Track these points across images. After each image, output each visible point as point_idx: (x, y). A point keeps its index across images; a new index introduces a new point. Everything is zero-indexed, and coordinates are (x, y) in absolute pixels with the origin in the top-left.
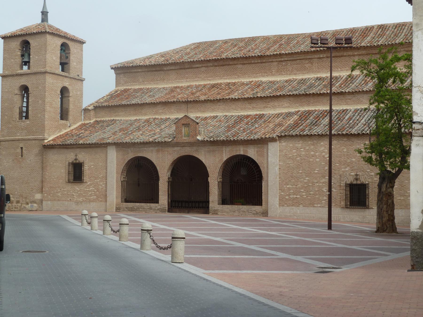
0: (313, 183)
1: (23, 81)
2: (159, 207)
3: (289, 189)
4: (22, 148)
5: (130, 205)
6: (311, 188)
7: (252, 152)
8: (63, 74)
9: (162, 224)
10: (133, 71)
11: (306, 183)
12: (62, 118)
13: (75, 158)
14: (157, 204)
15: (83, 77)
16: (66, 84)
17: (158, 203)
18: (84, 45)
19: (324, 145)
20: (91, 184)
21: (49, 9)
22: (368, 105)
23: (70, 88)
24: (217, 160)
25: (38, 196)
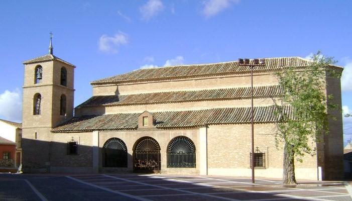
0: (229, 153)
1: (37, 90)
2: (127, 170)
3: (214, 157)
4: (36, 133)
5: (108, 168)
6: (227, 156)
7: (188, 134)
8: (61, 86)
9: (96, 184)
10: (130, 83)
11: (224, 153)
12: (61, 114)
13: (71, 139)
14: (126, 168)
15: (74, 88)
16: (64, 93)
17: (127, 167)
18: (75, 69)
19: (255, 125)
20: (82, 156)
21: (53, 47)
22: (122, 94)
23: (67, 95)
24: (166, 139)
25: (47, 164)
